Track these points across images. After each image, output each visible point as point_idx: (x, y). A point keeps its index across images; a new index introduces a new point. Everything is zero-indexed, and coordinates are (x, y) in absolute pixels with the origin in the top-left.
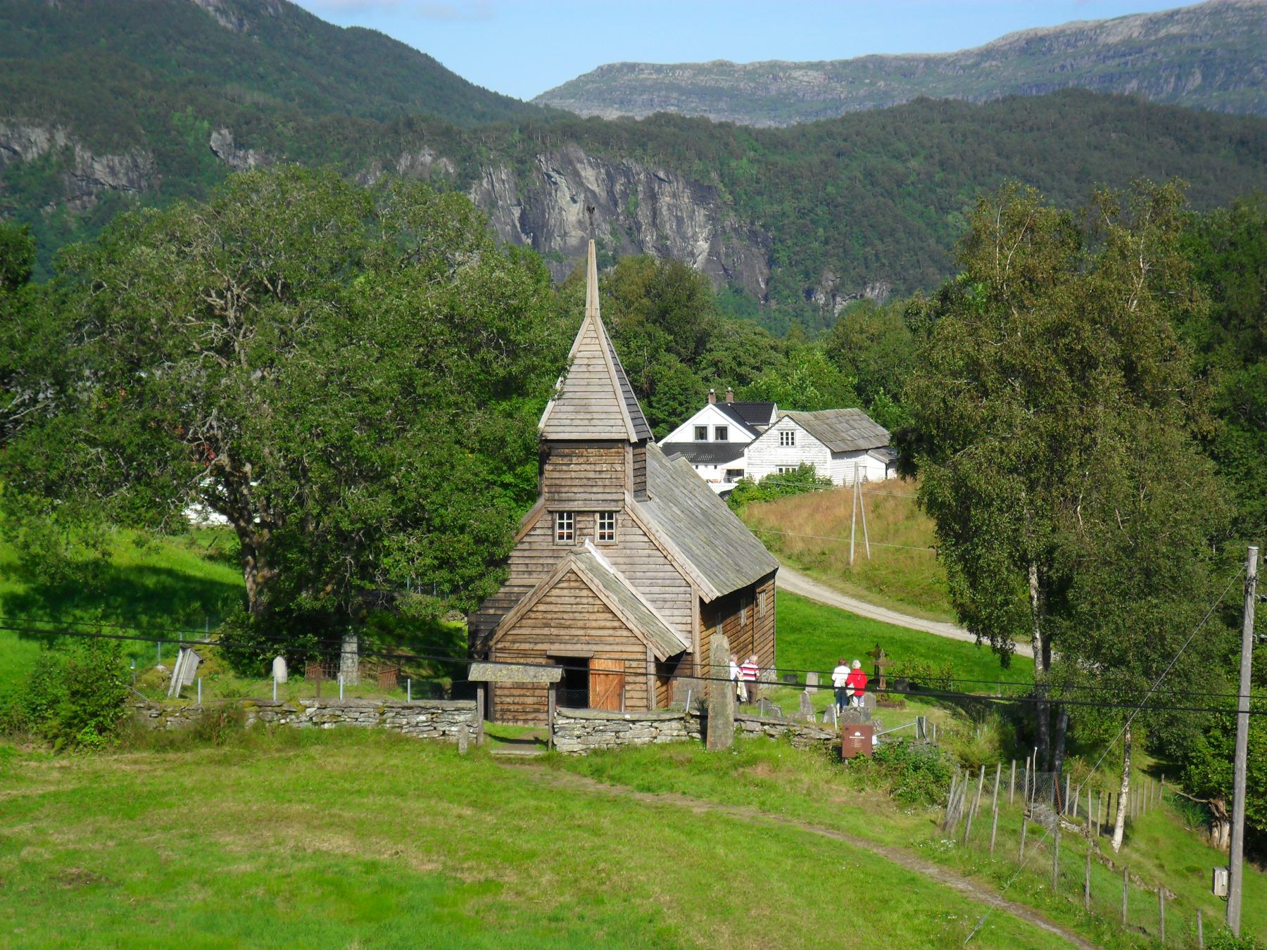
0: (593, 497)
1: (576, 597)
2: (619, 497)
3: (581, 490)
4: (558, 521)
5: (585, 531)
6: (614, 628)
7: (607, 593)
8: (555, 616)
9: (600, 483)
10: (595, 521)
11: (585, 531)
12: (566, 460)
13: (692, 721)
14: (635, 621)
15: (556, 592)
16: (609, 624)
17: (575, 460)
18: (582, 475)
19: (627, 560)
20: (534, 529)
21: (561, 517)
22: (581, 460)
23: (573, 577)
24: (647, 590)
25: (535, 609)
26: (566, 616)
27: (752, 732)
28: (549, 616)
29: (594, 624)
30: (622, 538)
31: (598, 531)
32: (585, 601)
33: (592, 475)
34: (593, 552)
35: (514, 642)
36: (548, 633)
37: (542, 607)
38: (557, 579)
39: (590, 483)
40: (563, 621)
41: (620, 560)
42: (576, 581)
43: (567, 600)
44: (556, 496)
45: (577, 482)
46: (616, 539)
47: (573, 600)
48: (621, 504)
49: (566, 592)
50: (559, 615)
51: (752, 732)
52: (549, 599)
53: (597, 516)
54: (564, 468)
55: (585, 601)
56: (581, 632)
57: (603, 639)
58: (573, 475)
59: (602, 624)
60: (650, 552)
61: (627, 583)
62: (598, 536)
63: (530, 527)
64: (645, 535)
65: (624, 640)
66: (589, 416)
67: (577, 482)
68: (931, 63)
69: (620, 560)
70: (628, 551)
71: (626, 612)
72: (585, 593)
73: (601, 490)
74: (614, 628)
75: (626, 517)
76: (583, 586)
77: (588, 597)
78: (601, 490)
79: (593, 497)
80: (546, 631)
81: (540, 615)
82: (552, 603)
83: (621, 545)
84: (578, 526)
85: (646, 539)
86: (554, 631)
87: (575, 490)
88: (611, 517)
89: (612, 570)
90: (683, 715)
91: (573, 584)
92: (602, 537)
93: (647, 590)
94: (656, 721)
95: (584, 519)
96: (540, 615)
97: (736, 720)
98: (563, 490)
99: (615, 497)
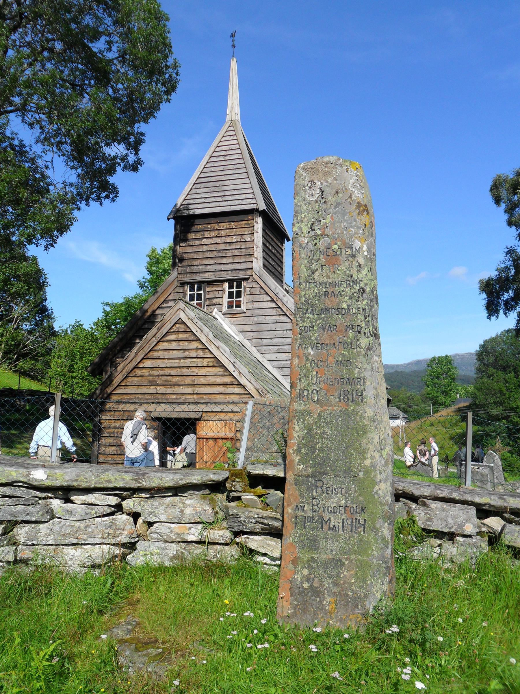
0: (223, 267)
1: (185, 350)
2: (248, 265)
3: (211, 262)
4: (189, 293)
5: (214, 301)
6: (225, 385)
7: (218, 343)
8: (161, 372)
9: (230, 254)
10: (223, 290)
11: (214, 301)
12: (199, 235)
13: (247, 496)
14: (249, 376)
15: (163, 346)
16: (219, 380)
17: (207, 234)
18: (213, 247)
19: (254, 328)
20: (166, 301)
21: (192, 289)
22: (213, 234)
23: (182, 328)
24: (273, 357)
25: (141, 365)
26: (173, 372)
27: (451, 536)
28: (155, 373)
29: (203, 380)
30: (250, 306)
31: (226, 299)
32: (193, 354)
33: (222, 247)
34: (220, 320)
35: (119, 402)
36: (154, 391)
37: (148, 363)
38: (164, 330)
39: (220, 254)
40: (169, 378)
41: (247, 328)
42: (185, 332)
43: (175, 354)
44: (188, 270)
45: (209, 255)
46: (243, 307)
47: (180, 354)
48: (249, 272)
49: (174, 345)
50: (166, 372)
51: (451, 536)
52: (155, 354)
53: (226, 285)
54: (197, 243)
55: (193, 354)
56: (189, 390)
57: (213, 397)
58: (205, 248)
59: (212, 380)
60: (277, 318)
61: (254, 350)
62: (225, 304)
63: (162, 299)
64: (273, 301)
65: (236, 398)
66: (222, 194)
67: (209, 255)
68: (398, 366)
69: (247, 328)
70: (256, 319)
71: (238, 364)
72: (194, 345)
73: (230, 260)
74: (225, 385)
75: (255, 285)
76: (192, 338)
77: (197, 349)
78: (230, 260)
79: (223, 267)
80: (152, 390)
81: (146, 372)
82: (159, 358)
83: (249, 313)
84: (207, 296)
85: (273, 305)
86: (161, 390)
87: (206, 262)
88: (239, 286)
89: (239, 337)
90: (219, 476)
91: (182, 336)
92: (230, 306)
93: (273, 357)
94: (135, 491)
95: (213, 289)
96: (146, 372)
97: (398, 496)
98: (195, 263)
99: (243, 266)
